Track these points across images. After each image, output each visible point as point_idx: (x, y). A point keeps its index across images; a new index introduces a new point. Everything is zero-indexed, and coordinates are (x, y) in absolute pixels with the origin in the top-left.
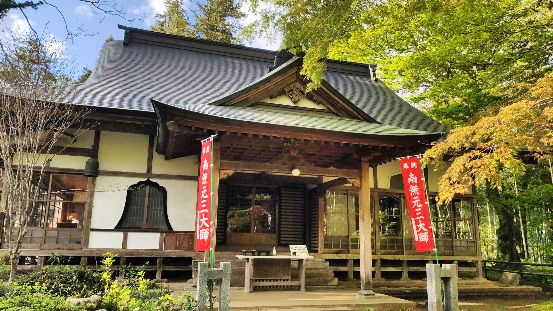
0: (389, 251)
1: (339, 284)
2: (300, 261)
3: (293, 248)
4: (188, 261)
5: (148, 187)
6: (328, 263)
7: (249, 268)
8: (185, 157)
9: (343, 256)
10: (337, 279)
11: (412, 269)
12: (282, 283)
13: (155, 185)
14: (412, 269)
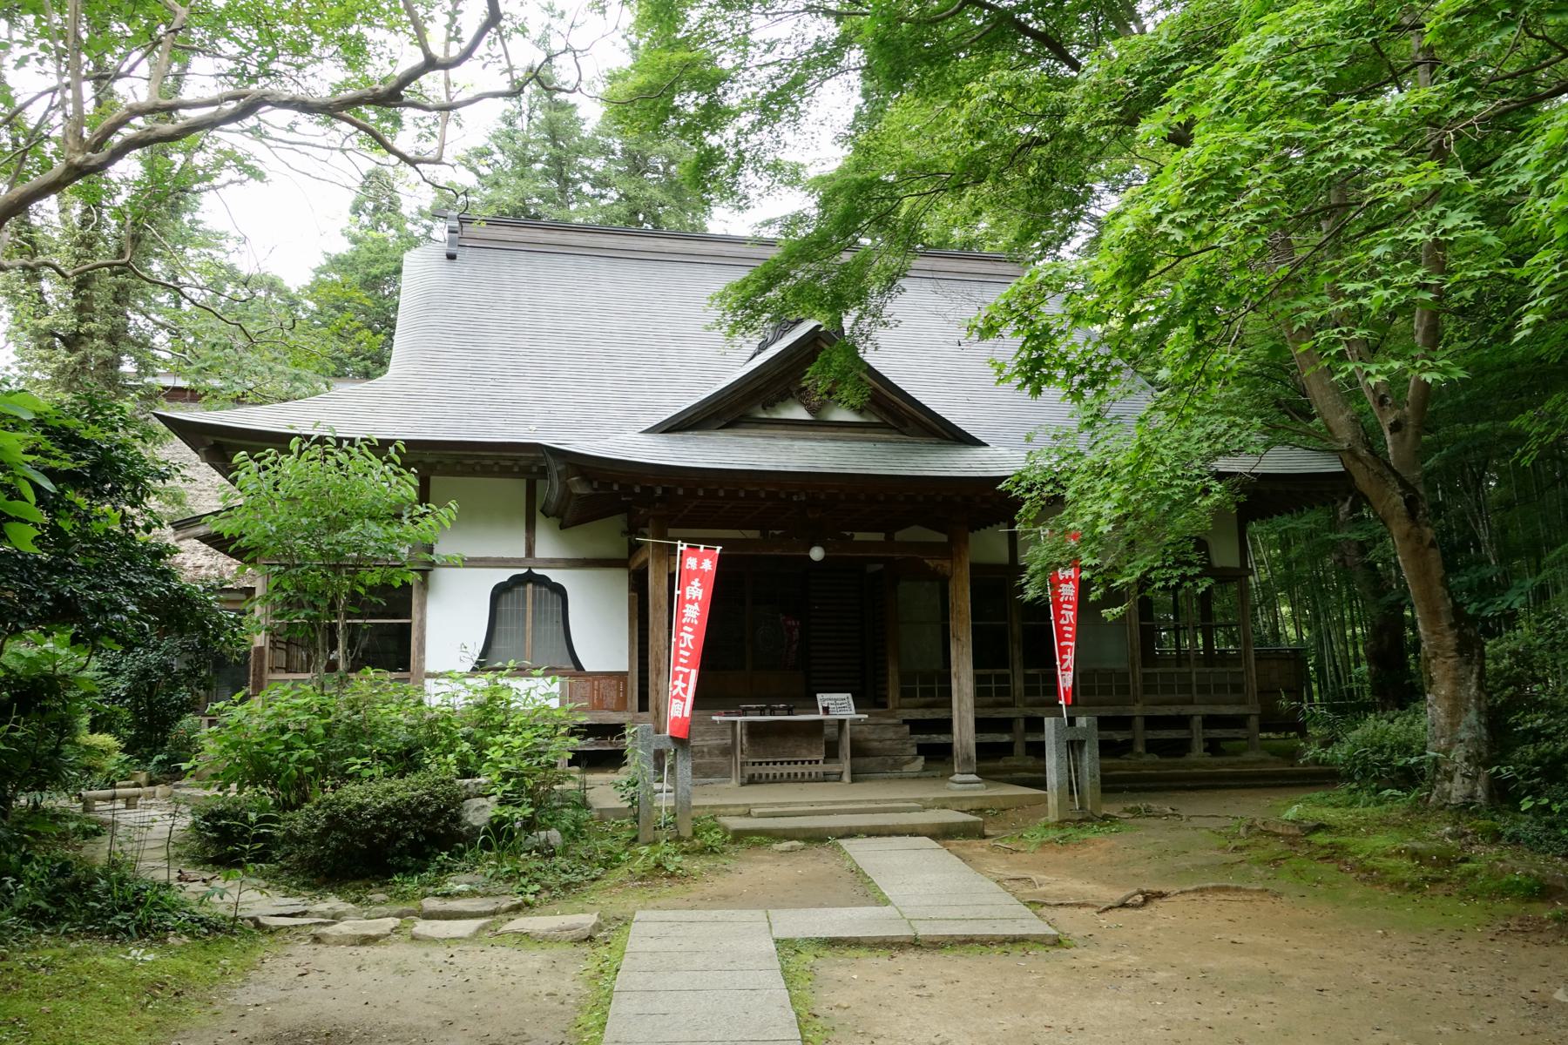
0: (1046, 698)
1: (925, 769)
2: (842, 722)
3: (823, 699)
4: (617, 730)
5: (530, 586)
6: (907, 728)
9: (1004, 713)
10: (922, 758)
12: (807, 768)
13: (543, 581)
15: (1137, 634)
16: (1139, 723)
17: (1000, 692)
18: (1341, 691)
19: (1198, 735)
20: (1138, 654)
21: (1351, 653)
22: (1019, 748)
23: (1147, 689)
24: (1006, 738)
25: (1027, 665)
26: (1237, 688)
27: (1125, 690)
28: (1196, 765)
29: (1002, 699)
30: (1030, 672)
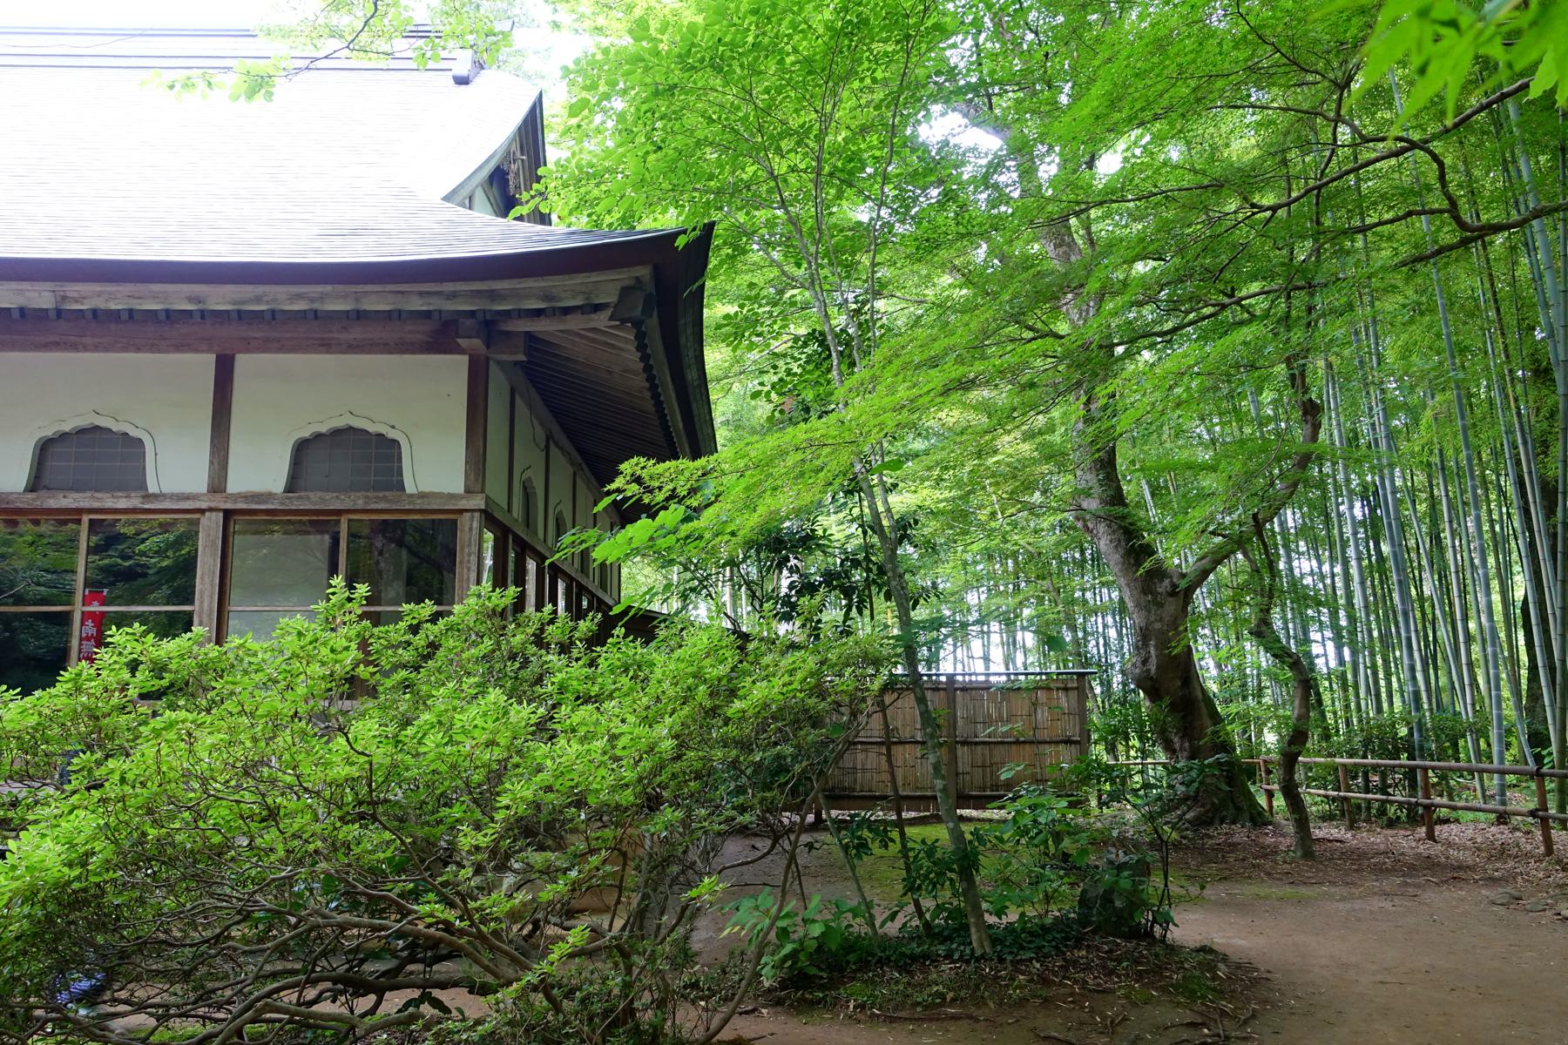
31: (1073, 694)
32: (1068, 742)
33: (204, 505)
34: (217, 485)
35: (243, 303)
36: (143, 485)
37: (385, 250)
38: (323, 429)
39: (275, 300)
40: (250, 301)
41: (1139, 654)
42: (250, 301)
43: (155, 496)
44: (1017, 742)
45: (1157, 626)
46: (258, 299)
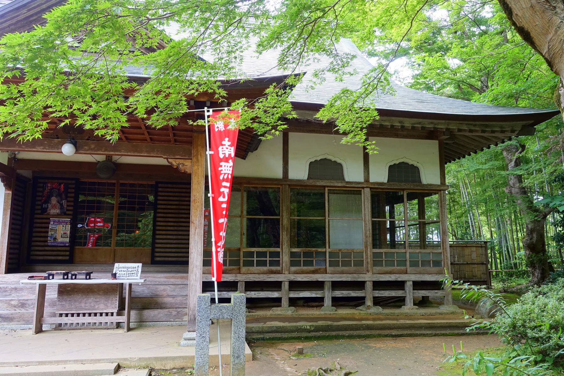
0: (305, 268)
3: (119, 267)
7: (51, 294)
8: (251, 79)
11: (339, 293)
14: (339, 293)
15: (370, 226)
16: (369, 286)
17: (272, 263)
18: (511, 264)
19: (409, 294)
20: (370, 240)
21: (516, 246)
22: (285, 302)
23: (376, 263)
24: (275, 295)
25: (292, 244)
26: (437, 263)
27: (359, 263)
28: (407, 316)
29: (274, 268)
30: (294, 250)
31: (484, 249)
32: (483, 264)
33: (365, 186)
34: (367, 180)
35: (415, 124)
36: (344, 179)
37: (466, 111)
38: (319, 159)
39: (424, 124)
40: (417, 123)
41: (529, 236)
42: (417, 123)
43: (347, 182)
44: (468, 264)
45: (538, 228)
46: (419, 123)
